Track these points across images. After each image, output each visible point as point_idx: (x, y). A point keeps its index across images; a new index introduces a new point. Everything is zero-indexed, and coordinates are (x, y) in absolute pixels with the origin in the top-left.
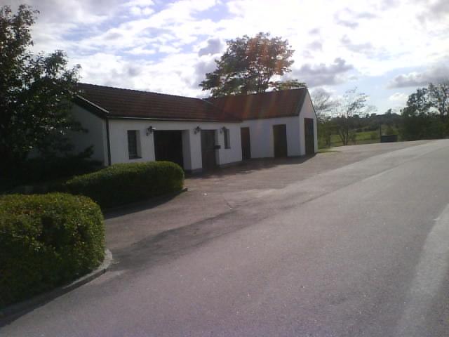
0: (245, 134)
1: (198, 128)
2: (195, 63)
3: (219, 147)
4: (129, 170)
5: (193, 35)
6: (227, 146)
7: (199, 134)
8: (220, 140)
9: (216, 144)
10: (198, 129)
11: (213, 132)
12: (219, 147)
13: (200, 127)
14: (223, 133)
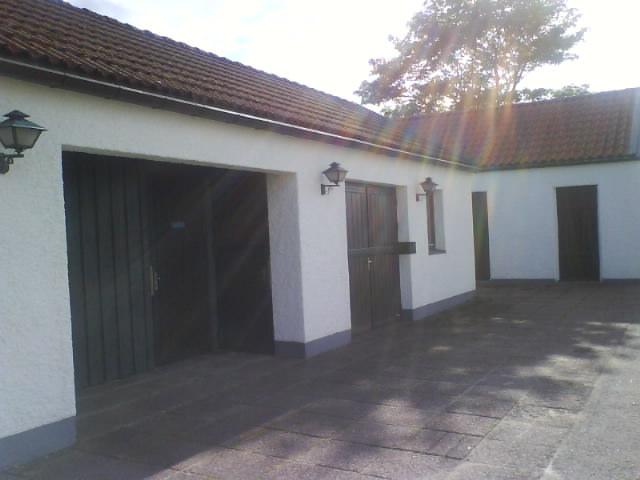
0: (479, 199)
1: (334, 166)
2: (394, 46)
3: (409, 248)
4: (241, 436)
5: (579, 36)
6: (434, 248)
7: (339, 195)
8: (415, 228)
9: (401, 239)
10: (334, 172)
11: (391, 192)
12: (409, 248)
13: (343, 166)
14: (424, 201)
